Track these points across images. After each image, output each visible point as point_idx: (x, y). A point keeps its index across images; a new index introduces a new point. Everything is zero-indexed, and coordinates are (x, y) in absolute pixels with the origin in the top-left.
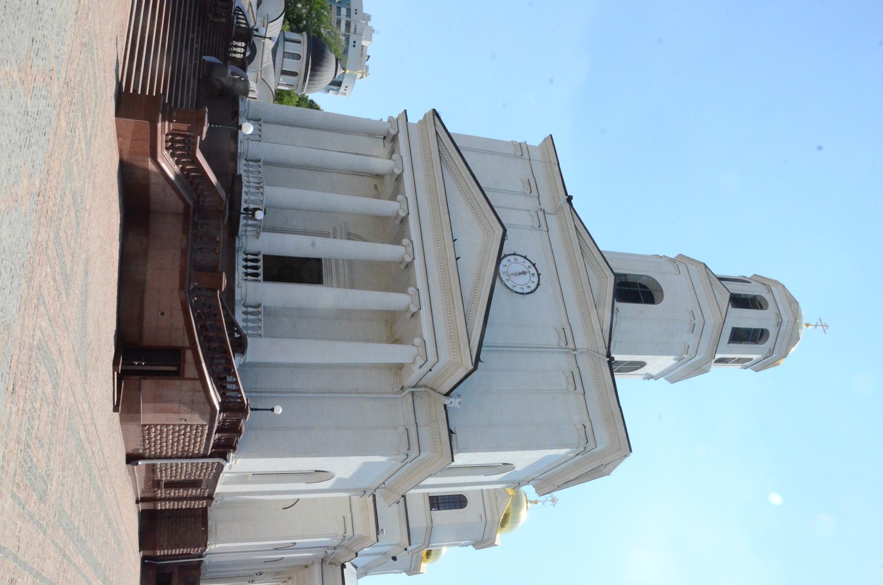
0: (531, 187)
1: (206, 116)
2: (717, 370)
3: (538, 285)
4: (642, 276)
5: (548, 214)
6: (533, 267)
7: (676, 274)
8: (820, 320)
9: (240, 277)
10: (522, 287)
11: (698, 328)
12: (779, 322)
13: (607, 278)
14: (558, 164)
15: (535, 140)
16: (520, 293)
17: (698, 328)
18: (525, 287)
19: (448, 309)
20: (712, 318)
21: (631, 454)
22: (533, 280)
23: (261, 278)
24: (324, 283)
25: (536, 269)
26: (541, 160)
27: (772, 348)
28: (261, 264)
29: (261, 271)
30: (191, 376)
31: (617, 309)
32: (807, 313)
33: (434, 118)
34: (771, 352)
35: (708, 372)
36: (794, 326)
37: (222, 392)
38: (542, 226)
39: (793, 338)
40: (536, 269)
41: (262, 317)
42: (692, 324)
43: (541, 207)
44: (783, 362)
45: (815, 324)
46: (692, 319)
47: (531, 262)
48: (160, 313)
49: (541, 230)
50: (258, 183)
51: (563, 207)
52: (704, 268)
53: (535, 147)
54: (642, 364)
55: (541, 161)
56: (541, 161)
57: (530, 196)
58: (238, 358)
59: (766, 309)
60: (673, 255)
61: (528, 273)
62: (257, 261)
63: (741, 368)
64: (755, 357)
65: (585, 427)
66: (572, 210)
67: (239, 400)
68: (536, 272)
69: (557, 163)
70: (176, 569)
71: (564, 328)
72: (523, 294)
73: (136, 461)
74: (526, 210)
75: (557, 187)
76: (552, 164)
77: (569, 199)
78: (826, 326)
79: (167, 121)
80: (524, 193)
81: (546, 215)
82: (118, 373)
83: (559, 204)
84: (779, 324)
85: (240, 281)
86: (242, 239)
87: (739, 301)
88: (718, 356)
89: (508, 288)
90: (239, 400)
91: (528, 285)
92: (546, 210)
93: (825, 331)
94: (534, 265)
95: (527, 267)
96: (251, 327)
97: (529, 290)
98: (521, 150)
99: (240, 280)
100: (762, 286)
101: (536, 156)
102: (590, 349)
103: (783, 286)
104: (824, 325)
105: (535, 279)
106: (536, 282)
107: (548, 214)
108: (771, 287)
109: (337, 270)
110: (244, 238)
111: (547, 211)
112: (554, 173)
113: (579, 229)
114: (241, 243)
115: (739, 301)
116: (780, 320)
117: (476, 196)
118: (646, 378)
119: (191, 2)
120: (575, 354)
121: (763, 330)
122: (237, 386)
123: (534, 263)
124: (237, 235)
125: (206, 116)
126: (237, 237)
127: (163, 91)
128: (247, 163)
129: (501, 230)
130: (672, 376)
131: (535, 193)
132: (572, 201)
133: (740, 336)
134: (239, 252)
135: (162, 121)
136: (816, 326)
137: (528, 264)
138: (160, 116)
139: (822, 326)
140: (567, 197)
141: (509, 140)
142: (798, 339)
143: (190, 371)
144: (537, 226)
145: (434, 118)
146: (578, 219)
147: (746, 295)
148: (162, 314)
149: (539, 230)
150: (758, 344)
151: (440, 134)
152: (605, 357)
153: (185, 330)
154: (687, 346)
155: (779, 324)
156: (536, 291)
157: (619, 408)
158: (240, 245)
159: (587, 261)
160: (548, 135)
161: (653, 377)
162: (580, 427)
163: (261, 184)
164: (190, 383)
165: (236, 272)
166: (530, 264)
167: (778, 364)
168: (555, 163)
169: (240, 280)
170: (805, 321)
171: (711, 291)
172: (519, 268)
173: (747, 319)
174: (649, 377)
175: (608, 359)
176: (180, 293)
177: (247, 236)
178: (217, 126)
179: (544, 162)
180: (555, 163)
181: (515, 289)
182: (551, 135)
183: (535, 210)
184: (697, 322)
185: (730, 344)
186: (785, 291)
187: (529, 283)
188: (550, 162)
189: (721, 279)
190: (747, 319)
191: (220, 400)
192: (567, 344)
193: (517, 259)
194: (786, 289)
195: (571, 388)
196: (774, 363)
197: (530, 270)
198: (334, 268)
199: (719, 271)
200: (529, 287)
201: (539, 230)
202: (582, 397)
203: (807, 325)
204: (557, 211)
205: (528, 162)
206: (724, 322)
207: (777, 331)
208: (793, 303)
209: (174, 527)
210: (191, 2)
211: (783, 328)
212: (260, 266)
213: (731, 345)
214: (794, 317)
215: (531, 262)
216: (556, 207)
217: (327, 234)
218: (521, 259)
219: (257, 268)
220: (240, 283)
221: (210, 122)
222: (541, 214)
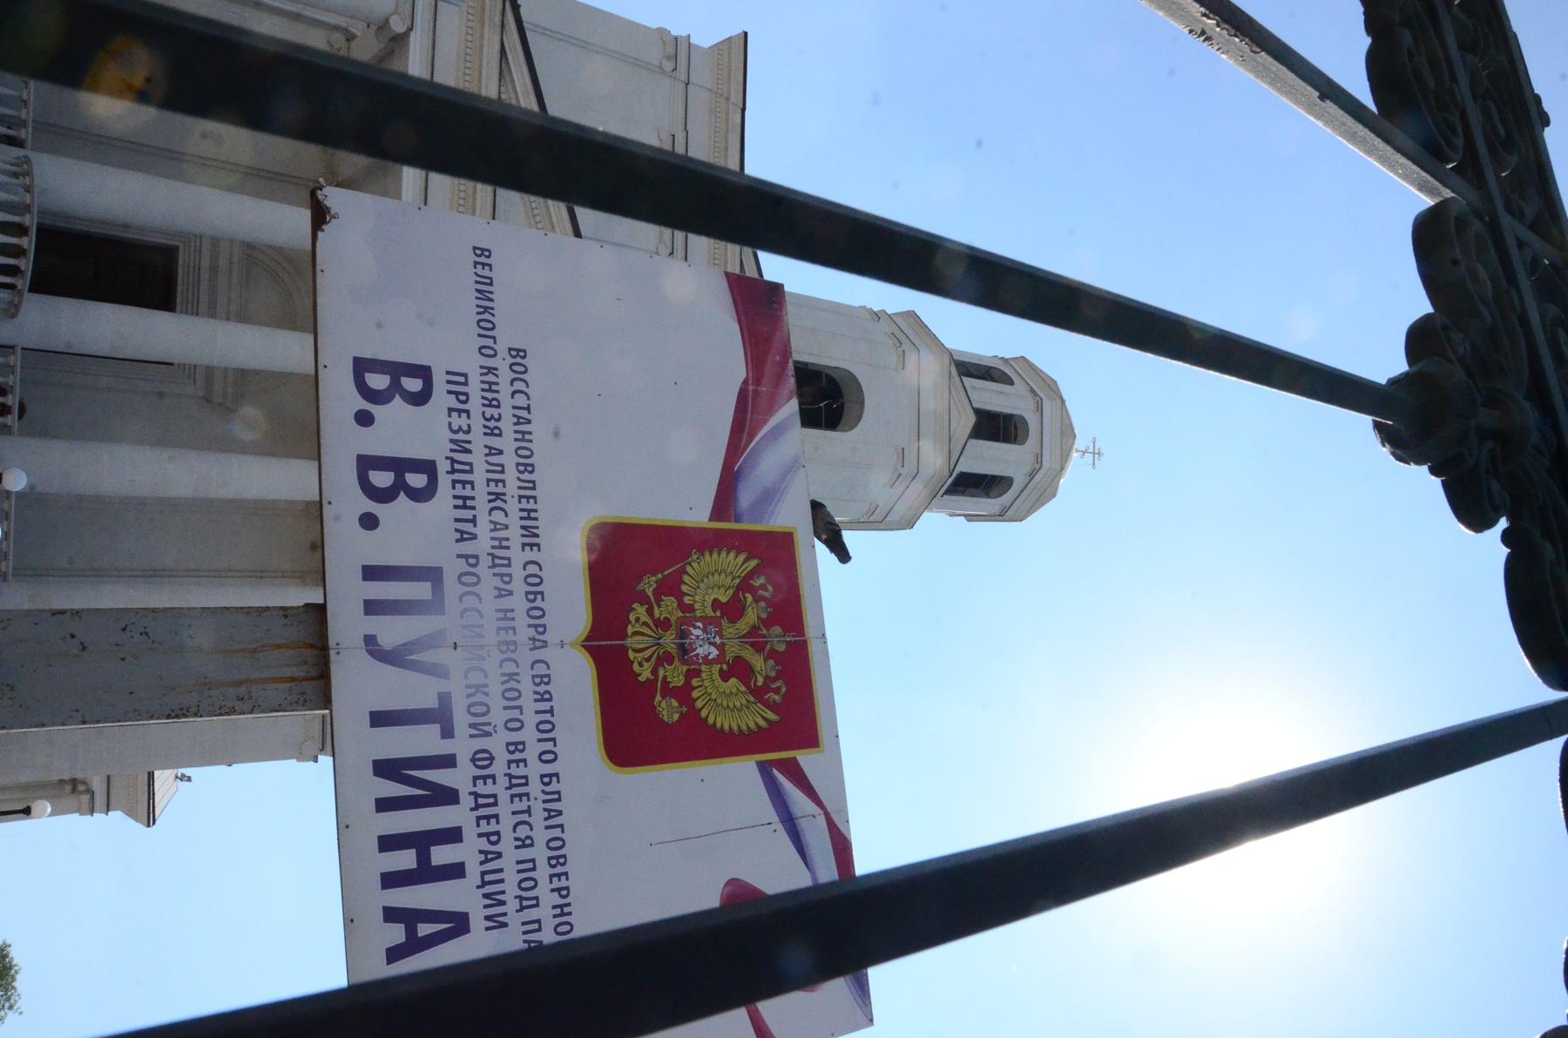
7: (896, 370)
19: (462, 195)
23: (22, 283)
24: (178, 308)
26: (710, 88)
27: (1008, 505)
28: (28, 242)
29: (26, 264)
33: (504, 8)
39: (1047, 493)
45: (1086, 454)
50: (16, 175)
56: (710, 90)
57: (671, 77)
59: (1022, 443)
62: (21, 230)
69: (741, 105)
71: (674, 135)
84: (1032, 475)
93: (1094, 464)
98: (676, 50)
100: (1029, 395)
101: (702, 75)
103: (1063, 401)
109: (213, 290)
112: (730, 127)
116: (1038, 466)
133: (971, 485)
136: (1084, 453)
139: (1094, 453)
141: (653, 24)
145: (504, 8)
151: (509, 56)
154: (874, 506)
155: (1032, 475)
160: (736, 31)
173: (988, 457)
188: (728, 99)
190: (988, 457)
198: (204, 285)
205: (681, 87)
207: (1027, 481)
208: (1067, 432)
211: (1038, 478)
212: (10, 407)
219: (19, 252)
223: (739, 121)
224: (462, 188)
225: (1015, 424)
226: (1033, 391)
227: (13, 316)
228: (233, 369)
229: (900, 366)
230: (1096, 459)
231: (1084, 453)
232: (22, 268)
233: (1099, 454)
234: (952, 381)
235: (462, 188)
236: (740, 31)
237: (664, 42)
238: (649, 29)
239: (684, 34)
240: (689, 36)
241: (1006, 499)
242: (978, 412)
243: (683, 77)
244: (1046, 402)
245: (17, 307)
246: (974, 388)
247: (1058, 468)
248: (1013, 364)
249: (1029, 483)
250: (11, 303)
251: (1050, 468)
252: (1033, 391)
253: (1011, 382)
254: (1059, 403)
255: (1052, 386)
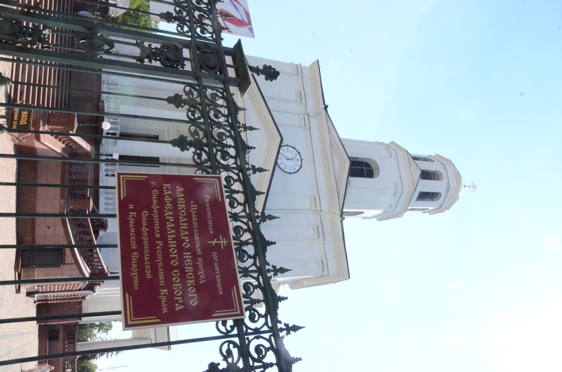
0: (302, 96)
1: (76, 118)
2: (408, 213)
3: (301, 167)
4: (368, 158)
5: (311, 116)
6: (298, 155)
8: (473, 183)
9: (103, 174)
10: (290, 168)
11: (398, 194)
12: (448, 189)
13: (345, 162)
14: (321, 82)
15: (307, 63)
16: (289, 173)
17: (398, 194)
18: (292, 169)
20: (408, 188)
21: (349, 279)
22: (298, 164)
25: (300, 156)
26: (309, 77)
27: (442, 204)
30: (70, 262)
31: (350, 182)
32: (465, 181)
34: (441, 206)
35: (401, 217)
36: (456, 191)
37: (89, 263)
38: (306, 124)
39: (455, 198)
40: (300, 156)
41: (119, 127)
42: (395, 191)
43: (307, 112)
44: (447, 211)
45: (469, 186)
46: (396, 188)
47: (297, 151)
48: (46, 227)
49: (306, 128)
51: (321, 113)
52: (407, 154)
53: (306, 67)
54: (362, 213)
55: (310, 78)
56: (310, 78)
58: (101, 232)
60: (387, 142)
61: (295, 159)
63: (422, 213)
64: (431, 208)
65: (323, 262)
66: (327, 115)
67: (100, 267)
68: (300, 158)
70: (62, 327)
71: (318, 226)
72: (290, 173)
73: (33, 295)
74: (297, 114)
75: (318, 97)
76: (317, 81)
77: (326, 107)
78: (475, 187)
79: (46, 125)
80: (297, 101)
81: (309, 117)
82: (18, 273)
83: (319, 110)
84: (448, 190)
85: (103, 178)
86: (104, 146)
87: (426, 175)
88: (409, 208)
89: (281, 169)
90: (100, 267)
91: (294, 167)
92: (310, 114)
93: (474, 190)
94: (299, 153)
95: (295, 155)
96: (110, 203)
97: (295, 171)
99: (103, 176)
100: (441, 164)
102: (330, 210)
103: (454, 165)
104: (474, 186)
105: (299, 163)
106: (300, 165)
107: (311, 116)
108: (446, 165)
110: (106, 145)
111: (311, 115)
113: (330, 129)
114: (103, 149)
115: (426, 175)
116: (449, 187)
117: (265, 113)
118: (364, 218)
119: (64, 1)
120: (320, 214)
121: (437, 193)
122: (99, 260)
123: (299, 152)
124: (101, 144)
125: (76, 118)
126: (101, 145)
127: (49, 8)
128: (108, 86)
129: (280, 139)
130: (380, 218)
131: (303, 102)
132: (328, 109)
133: (425, 196)
134: (104, 83)
135: (43, 126)
136: (469, 187)
137: (295, 152)
138: (41, 122)
139: (473, 187)
140: (324, 106)
142: (458, 198)
143: (69, 259)
144: (303, 125)
146: (330, 121)
147: (430, 170)
148: (49, 228)
149: (304, 128)
150: (434, 201)
152: (339, 217)
153: (65, 237)
155: (448, 190)
156: (299, 171)
157: (344, 250)
158: (103, 151)
159: (333, 149)
160: (315, 60)
161: (368, 218)
162: (320, 262)
163: (118, 106)
164: (70, 266)
165: (100, 171)
166: (297, 153)
167: (444, 212)
168: (319, 81)
169: (103, 176)
170: (463, 184)
171: (409, 170)
172: (290, 156)
173: (428, 186)
174: (365, 218)
175: (341, 219)
176: (61, 209)
177: (108, 144)
178: (84, 125)
179: (312, 79)
180: (319, 81)
181: (286, 170)
182: (318, 60)
183: (303, 114)
184: (398, 190)
185: (417, 201)
186: (454, 168)
187: (294, 154)
188: (316, 80)
189: (415, 158)
190: (428, 186)
191: (90, 271)
192: (316, 208)
193: (288, 149)
194: (455, 167)
195: (316, 237)
196: (443, 211)
197: (296, 157)
199: (414, 152)
200: (295, 168)
201: (304, 128)
202: (322, 242)
203: (465, 186)
204: (317, 115)
206: (415, 190)
207: (446, 193)
208: (458, 176)
209: (60, 308)
210: (64, 1)
211: (450, 191)
213: (417, 202)
214: (457, 186)
215: (297, 151)
216: (317, 112)
217: (163, 131)
218: (291, 149)
220: (103, 179)
221: (79, 123)
222: (306, 116)
223: (320, 85)
224: (233, 89)
225: (437, 174)
226: (441, 163)
227: (116, 145)
228: (176, 158)
229: (390, 157)
230: (475, 189)
231: (469, 187)
232: (117, 133)
233: (475, 187)
234: (409, 159)
235: (233, 89)
236: (316, 60)
237: (314, 229)
238: (288, 63)
239: (299, 63)
240: (301, 64)
241: (440, 201)
242: (421, 170)
243: (308, 127)
244: (447, 166)
245: (116, 143)
246: (419, 163)
247: (457, 187)
248: (435, 157)
249: (447, 194)
250: (115, 142)
251: (454, 188)
252: (441, 163)
253: (434, 161)
254: (452, 165)
255: (449, 161)
